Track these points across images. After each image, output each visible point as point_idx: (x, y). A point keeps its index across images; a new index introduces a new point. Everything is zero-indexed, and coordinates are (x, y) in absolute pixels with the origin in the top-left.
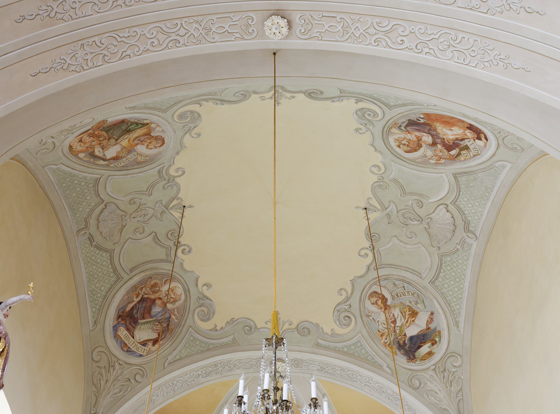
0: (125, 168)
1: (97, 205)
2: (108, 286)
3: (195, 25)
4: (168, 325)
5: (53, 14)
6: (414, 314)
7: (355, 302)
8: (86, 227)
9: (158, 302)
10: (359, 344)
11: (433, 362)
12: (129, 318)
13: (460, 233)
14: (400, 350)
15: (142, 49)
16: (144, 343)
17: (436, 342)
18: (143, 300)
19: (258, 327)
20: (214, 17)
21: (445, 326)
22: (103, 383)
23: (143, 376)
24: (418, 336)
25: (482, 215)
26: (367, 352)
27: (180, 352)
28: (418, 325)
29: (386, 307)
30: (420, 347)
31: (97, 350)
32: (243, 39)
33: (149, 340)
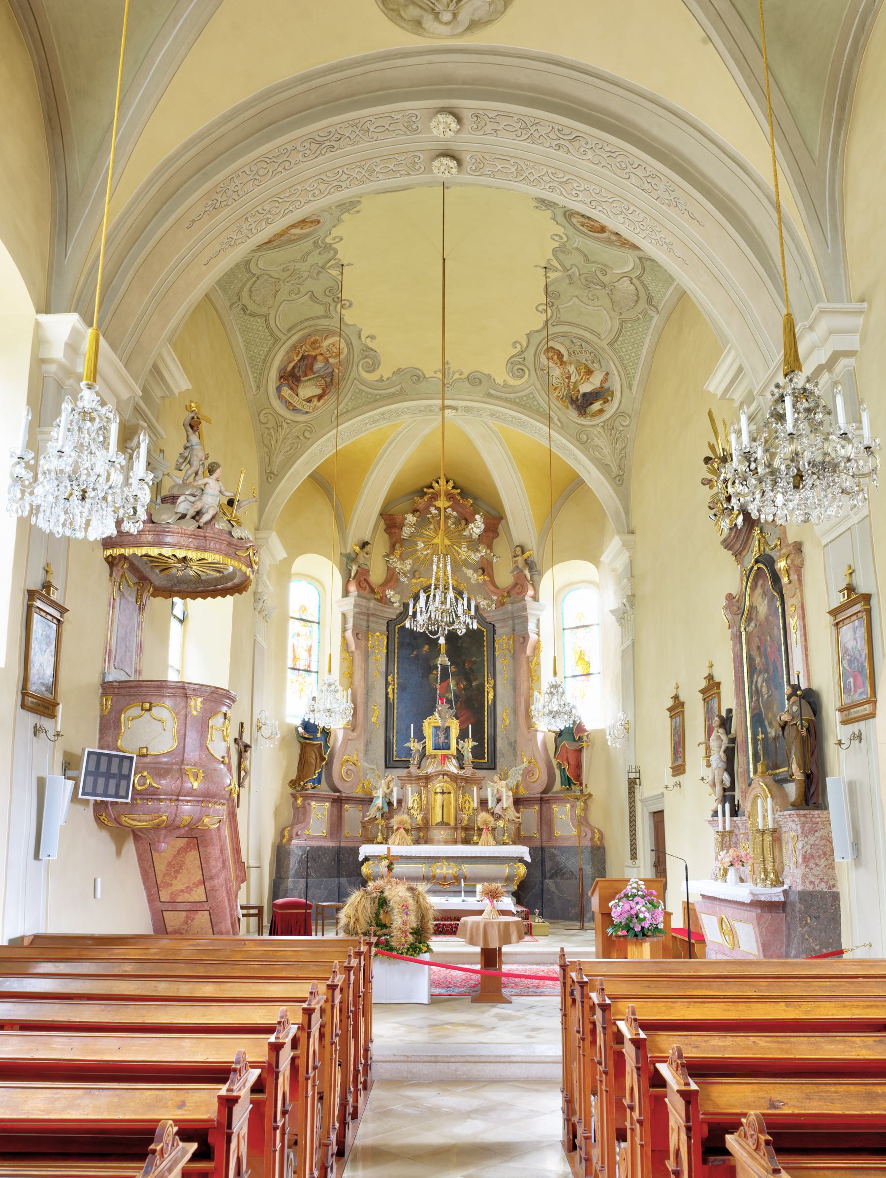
0: (279, 246)
1: (248, 280)
2: (267, 349)
3: (357, 170)
4: (332, 379)
5: (218, 205)
6: (589, 372)
7: (530, 355)
8: (239, 299)
9: (320, 358)
10: (531, 396)
11: (602, 420)
12: (291, 377)
13: (643, 304)
14: (572, 404)
15: (303, 202)
16: (309, 400)
17: (608, 401)
18: (303, 358)
19: (427, 376)
20: (378, 160)
21: (619, 387)
22: (273, 443)
23: (311, 432)
24: (590, 394)
25: (665, 295)
26: (539, 404)
27: (347, 405)
28: (592, 383)
29: (562, 363)
30: (592, 404)
31: (264, 412)
32: (409, 175)
33: (313, 397)
